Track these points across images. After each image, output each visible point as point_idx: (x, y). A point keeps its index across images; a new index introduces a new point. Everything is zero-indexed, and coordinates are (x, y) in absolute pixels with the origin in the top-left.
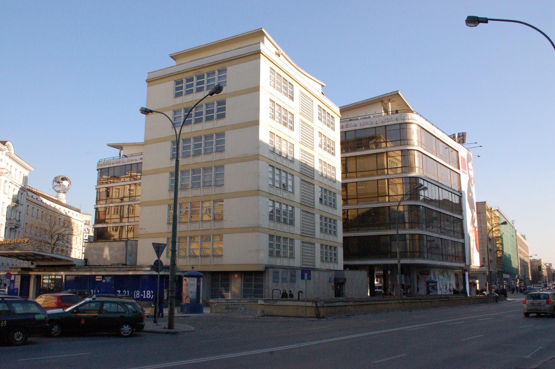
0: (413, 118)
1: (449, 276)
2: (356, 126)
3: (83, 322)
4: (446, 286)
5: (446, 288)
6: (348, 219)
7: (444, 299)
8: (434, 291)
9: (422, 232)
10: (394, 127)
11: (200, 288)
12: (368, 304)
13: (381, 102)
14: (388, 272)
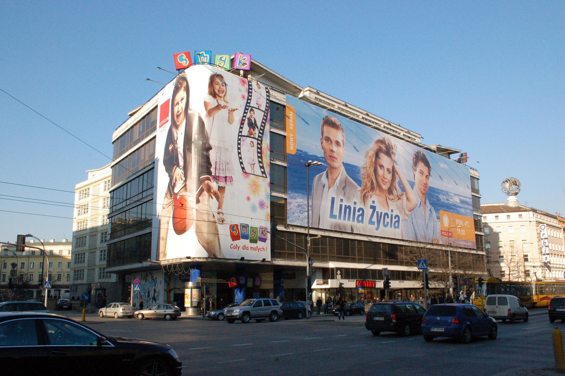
1: (154, 280)
3: (354, 310)
4: (149, 293)
5: (149, 295)
11: (334, 273)
14: (438, 320)
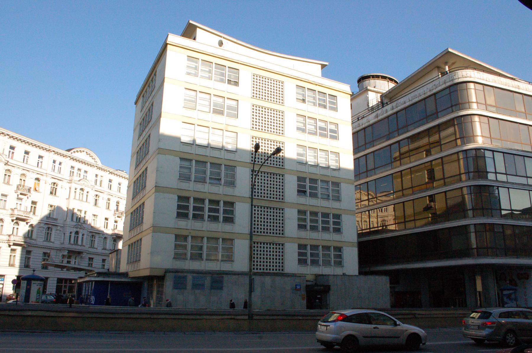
0: (466, 76)
2: (405, 103)
6: (436, 213)
7: (309, 318)
8: (509, 301)
9: (488, 220)
10: (443, 93)
12: (407, 318)
13: (437, 69)
